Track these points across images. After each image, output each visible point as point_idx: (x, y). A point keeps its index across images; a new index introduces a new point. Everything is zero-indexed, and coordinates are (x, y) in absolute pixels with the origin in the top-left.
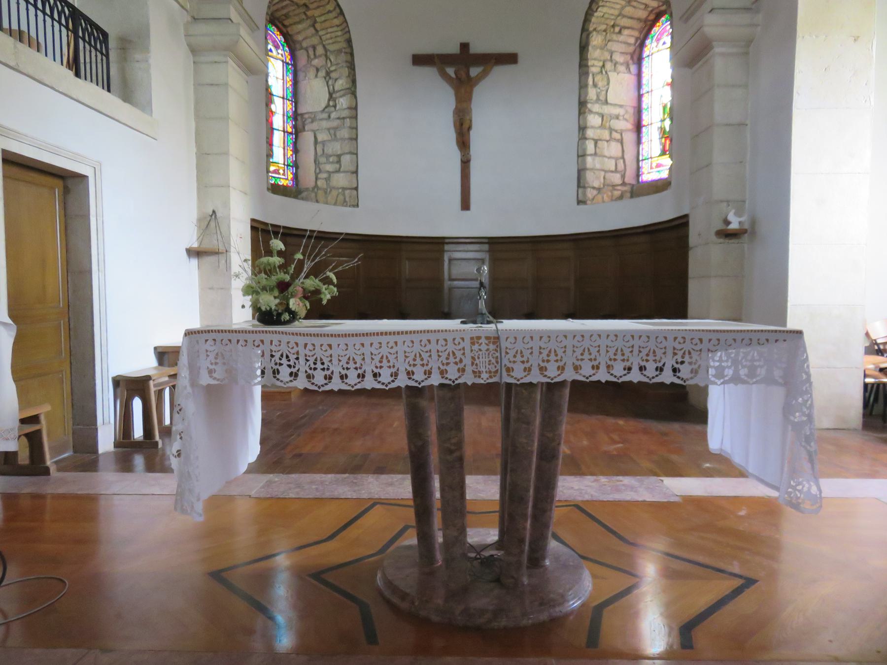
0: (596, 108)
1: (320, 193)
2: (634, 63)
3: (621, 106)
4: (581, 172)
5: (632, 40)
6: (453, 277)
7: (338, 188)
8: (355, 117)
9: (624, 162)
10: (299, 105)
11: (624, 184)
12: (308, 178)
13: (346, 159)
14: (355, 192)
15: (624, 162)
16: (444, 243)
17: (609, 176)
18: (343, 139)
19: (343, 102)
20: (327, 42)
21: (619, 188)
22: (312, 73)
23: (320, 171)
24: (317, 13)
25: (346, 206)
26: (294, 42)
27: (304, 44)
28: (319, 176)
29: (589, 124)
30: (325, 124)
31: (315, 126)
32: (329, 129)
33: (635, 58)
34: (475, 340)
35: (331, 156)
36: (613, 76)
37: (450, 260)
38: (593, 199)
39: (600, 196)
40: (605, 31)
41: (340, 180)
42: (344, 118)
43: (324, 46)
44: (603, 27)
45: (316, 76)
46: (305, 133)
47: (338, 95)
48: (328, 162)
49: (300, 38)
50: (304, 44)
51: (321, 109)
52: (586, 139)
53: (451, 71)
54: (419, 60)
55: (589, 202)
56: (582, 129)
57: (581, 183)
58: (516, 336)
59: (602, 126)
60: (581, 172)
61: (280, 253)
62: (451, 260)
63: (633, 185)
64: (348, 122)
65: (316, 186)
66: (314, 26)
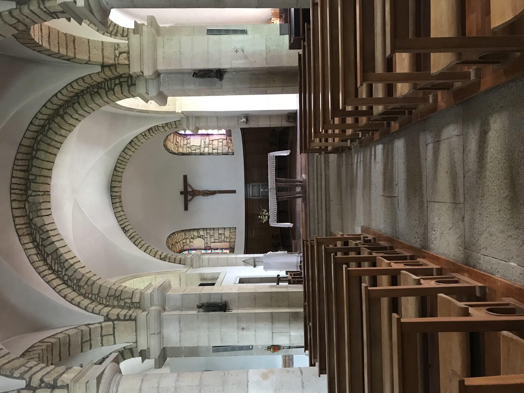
3: (201, 141)
4: (223, 154)
5: (180, 138)
7: (230, 234)
9: (219, 139)
10: (202, 248)
11: (226, 139)
12: (227, 245)
13: (220, 232)
15: (219, 139)
17: (224, 144)
21: (228, 141)
23: (224, 241)
24: (174, 241)
26: (181, 249)
30: (208, 239)
31: (209, 243)
32: (210, 238)
33: (185, 136)
34: (271, 191)
36: (191, 144)
37: (253, 197)
39: (231, 147)
41: (227, 233)
42: (207, 233)
43: (183, 240)
44: (177, 148)
45: (192, 242)
47: (199, 235)
48: (221, 238)
50: (182, 246)
53: (189, 197)
54: (186, 208)
55: (233, 151)
56: (209, 154)
57: (227, 154)
59: (208, 147)
60: (223, 154)
61: (260, 217)
64: (208, 231)
66: (177, 243)
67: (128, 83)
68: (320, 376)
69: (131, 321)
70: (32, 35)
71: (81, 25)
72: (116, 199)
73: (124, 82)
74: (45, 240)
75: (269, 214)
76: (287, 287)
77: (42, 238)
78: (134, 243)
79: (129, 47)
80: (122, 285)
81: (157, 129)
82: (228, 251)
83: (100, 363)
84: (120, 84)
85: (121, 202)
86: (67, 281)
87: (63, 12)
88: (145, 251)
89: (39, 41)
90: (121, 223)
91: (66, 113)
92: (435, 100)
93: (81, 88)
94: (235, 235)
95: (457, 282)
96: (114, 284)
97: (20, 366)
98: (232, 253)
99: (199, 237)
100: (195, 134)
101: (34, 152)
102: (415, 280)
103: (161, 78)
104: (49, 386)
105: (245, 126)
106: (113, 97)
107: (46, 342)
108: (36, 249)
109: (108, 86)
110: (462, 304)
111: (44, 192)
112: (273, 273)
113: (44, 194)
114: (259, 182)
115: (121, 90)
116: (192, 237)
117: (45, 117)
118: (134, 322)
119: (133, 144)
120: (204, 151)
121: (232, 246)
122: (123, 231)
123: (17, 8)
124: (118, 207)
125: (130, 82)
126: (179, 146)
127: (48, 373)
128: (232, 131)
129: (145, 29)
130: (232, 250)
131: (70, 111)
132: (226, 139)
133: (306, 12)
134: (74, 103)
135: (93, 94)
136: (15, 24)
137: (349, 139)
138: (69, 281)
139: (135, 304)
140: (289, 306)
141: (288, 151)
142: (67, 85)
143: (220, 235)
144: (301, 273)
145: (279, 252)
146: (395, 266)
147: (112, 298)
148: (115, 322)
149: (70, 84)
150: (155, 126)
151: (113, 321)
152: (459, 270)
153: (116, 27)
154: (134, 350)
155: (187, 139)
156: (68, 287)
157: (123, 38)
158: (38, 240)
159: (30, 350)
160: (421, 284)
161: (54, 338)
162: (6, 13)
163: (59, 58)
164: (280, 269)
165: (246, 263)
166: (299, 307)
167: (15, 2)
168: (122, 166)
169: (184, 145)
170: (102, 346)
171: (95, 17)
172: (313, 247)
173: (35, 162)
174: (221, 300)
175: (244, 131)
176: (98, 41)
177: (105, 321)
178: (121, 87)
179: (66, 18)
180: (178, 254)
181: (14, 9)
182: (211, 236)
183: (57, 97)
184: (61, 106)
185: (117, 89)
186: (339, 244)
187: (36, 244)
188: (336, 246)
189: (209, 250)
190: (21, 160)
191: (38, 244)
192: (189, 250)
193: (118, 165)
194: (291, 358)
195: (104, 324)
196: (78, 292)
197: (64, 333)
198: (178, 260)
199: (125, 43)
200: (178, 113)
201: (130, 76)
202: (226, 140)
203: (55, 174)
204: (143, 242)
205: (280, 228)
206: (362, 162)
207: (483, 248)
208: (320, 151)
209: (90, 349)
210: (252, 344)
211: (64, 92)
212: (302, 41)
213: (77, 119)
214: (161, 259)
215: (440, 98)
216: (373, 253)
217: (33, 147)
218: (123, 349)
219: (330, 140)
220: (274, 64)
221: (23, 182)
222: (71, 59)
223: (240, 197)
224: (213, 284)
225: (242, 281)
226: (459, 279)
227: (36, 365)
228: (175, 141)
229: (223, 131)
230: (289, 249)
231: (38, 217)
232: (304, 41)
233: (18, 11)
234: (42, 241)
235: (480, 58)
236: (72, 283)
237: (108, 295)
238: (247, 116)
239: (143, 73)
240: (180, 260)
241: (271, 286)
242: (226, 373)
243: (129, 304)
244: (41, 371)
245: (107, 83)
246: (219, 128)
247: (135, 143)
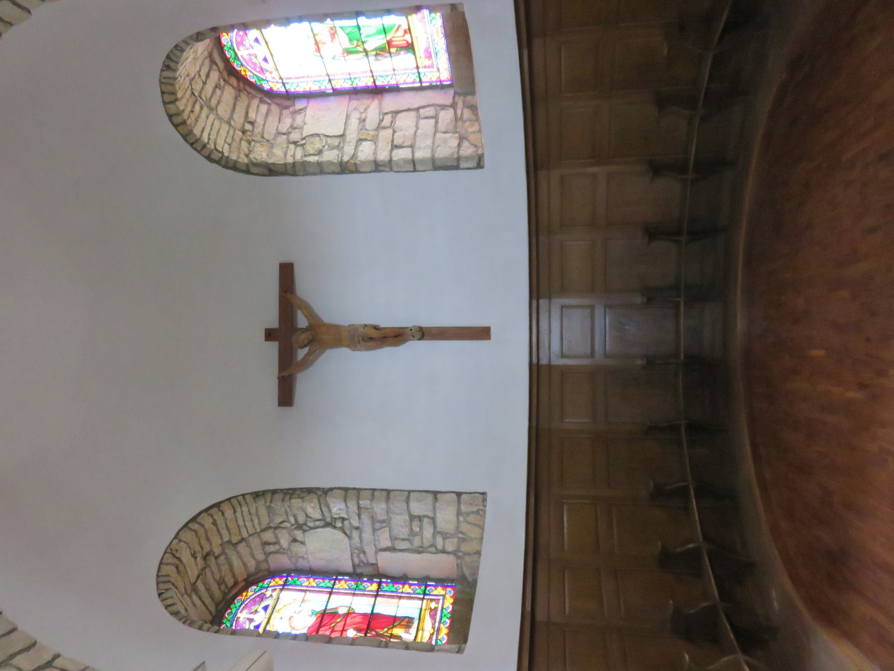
0: (349, 150)
1: (465, 548)
3: (348, 117)
4: (437, 165)
5: (264, 108)
9: (423, 107)
11: (454, 106)
12: (444, 564)
13: (417, 508)
14: (463, 497)
15: (423, 107)
21: (459, 112)
22: (297, 548)
24: (216, 541)
26: (258, 570)
28: (440, 547)
30: (367, 535)
31: (370, 550)
32: (374, 530)
33: (287, 103)
38: (476, 146)
40: (249, 142)
41: (446, 517)
42: (359, 508)
43: (263, 530)
44: (244, 144)
45: (303, 543)
46: (379, 565)
47: (327, 514)
50: (261, 557)
51: (346, 539)
52: (391, 160)
54: (286, 397)
55: (480, 152)
56: (377, 167)
57: (453, 165)
59: (374, 140)
60: (437, 165)
62: (563, 356)
65: (454, 553)
94: (482, 528)
99: (327, 525)
116: (301, 519)
121: (467, 572)
126: (258, 138)
132: (454, 106)
143: (416, 524)
155: (296, 112)
174: (447, 113)
182: (378, 525)
202: (451, 111)
228: (239, 118)
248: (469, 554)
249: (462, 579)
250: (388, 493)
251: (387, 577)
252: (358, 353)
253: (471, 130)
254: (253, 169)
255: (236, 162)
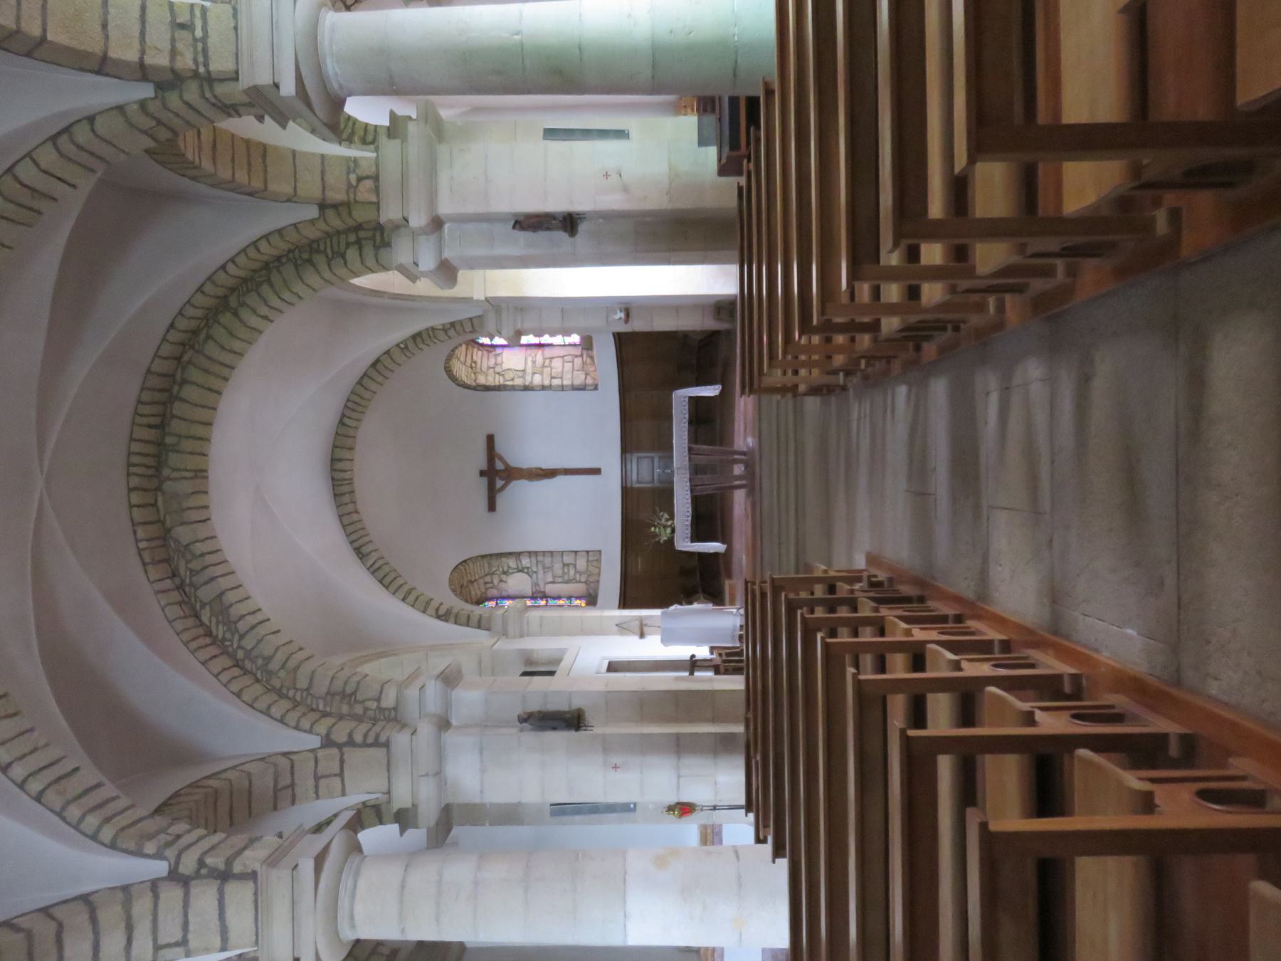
0: (528, 378)
1: (591, 579)
2: (495, 350)
3: (526, 359)
5: (480, 353)
6: (650, 479)
7: (588, 566)
8: (536, 553)
9: (566, 356)
11: (582, 356)
12: (580, 588)
13: (567, 559)
14: (590, 553)
15: (566, 356)
16: (626, 487)
18: (552, 562)
19: (526, 562)
20: (483, 573)
22: (503, 585)
25: (600, 559)
27: (483, 590)
28: (578, 580)
29: (541, 384)
30: (541, 575)
31: (541, 584)
32: (544, 573)
33: (491, 349)
34: (677, 474)
35: (564, 571)
36: (505, 366)
38: (594, 379)
39: (591, 373)
40: (475, 374)
41: (582, 563)
42: (537, 562)
44: (473, 375)
45: (505, 582)
46: (546, 592)
47: (520, 566)
49: (479, 593)
50: (483, 590)
51: (529, 578)
52: (551, 385)
53: (499, 483)
54: (492, 507)
55: (596, 382)
56: (543, 388)
57: (582, 388)
58: (676, 465)
59: (541, 373)
60: (574, 388)
61: (655, 528)
62: (638, 482)
63: (583, 349)
64: (540, 558)
65: (585, 582)
67: (375, 242)
68: (774, 862)
69: (378, 747)
70: (182, 145)
71: (284, 127)
72: (342, 485)
73: (366, 239)
74: (198, 572)
75: (673, 523)
76: (710, 680)
77: (191, 571)
78: (381, 582)
79: (377, 166)
80: (358, 670)
81: (431, 334)
82: (583, 603)
83: (319, 828)
84: (359, 243)
85: (353, 492)
86: (243, 661)
87: (251, 105)
88: (404, 600)
89: (194, 159)
90: (354, 537)
91: (242, 304)
92: (1001, 308)
93: (276, 253)
94: (599, 568)
95: (1032, 666)
96: (342, 669)
97: (158, 833)
98: (591, 607)
100: (514, 342)
101: (176, 388)
102: (950, 661)
103: (446, 231)
104: (215, 874)
105: (623, 328)
106: (341, 271)
107: (203, 787)
108: (180, 592)
109: (332, 247)
110: (1026, 706)
111: (196, 471)
112: (682, 652)
113: (196, 475)
114: (652, 449)
115: (361, 255)
117: (199, 313)
118: (384, 750)
119: (379, 366)
120: (532, 381)
121: (591, 592)
122: (358, 555)
123: (156, 97)
124: (346, 504)
125: (378, 238)
127: (213, 848)
128: (593, 337)
129: (412, 128)
130: (592, 600)
131: (252, 299)
132: (582, 356)
133: (753, 103)
134: (261, 284)
135: (301, 265)
136: (151, 128)
137: (841, 370)
138: (247, 661)
139: (387, 712)
140: (714, 720)
141: (717, 387)
142: (248, 246)
144: (742, 650)
145: (696, 606)
146: (919, 634)
147: (337, 697)
148: (346, 749)
149: (254, 244)
150: (427, 329)
151: (340, 747)
152: (1039, 644)
153: (350, 124)
154: (383, 808)
156: (245, 674)
157: (365, 147)
158: (182, 572)
159: (170, 802)
160: (960, 669)
161: (219, 779)
162: (135, 107)
163: (232, 190)
164: (698, 641)
165: (623, 628)
166: (734, 721)
167: (152, 84)
168: (354, 415)
169: (489, 368)
170: (318, 797)
171: (316, 115)
172: (763, 595)
173: (178, 409)
174: (570, 706)
175: (622, 340)
176: (313, 154)
177: (323, 746)
178: (360, 249)
179: (256, 117)
180: (474, 608)
181: (152, 99)
183: (226, 272)
184: (233, 290)
185: (352, 254)
186: (819, 591)
187: (177, 581)
188: (812, 593)
189: (542, 598)
190: (148, 404)
191: (183, 582)
192: (497, 598)
193: (348, 413)
194: (717, 830)
195: (320, 754)
196: (266, 685)
197: (238, 768)
198: (474, 619)
199: (371, 158)
200: (478, 301)
201: (379, 228)
203: (217, 434)
204: (400, 581)
205: (699, 554)
206: (868, 418)
207: (1083, 601)
208: (783, 390)
209: (293, 802)
210: (635, 801)
211: (241, 260)
212: (745, 162)
213: (265, 318)
214: (439, 617)
215: (1008, 305)
216: (881, 610)
217: (173, 376)
218: (360, 806)
219: (803, 372)
220: (686, 203)
221: (151, 449)
222: (256, 192)
223: (609, 488)
224: (552, 673)
225: (613, 667)
226: (1036, 660)
227: (189, 831)
229: (575, 338)
230: (716, 596)
231: (182, 524)
232: (749, 161)
233: (158, 102)
234: (191, 576)
235: (1063, 249)
236: (254, 666)
237: (328, 693)
238: (628, 307)
239: (408, 222)
240: (479, 621)
241: (677, 679)
242: (580, 855)
243: (373, 712)
244: (199, 844)
245: (331, 241)
246: (567, 333)
247: (385, 366)
248: (593, 582)
249: (590, 595)
250: (552, 553)
251: (550, 597)
252: (532, 483)
253: (591, 370)
254: (478, 388)
255: (470, 385)
